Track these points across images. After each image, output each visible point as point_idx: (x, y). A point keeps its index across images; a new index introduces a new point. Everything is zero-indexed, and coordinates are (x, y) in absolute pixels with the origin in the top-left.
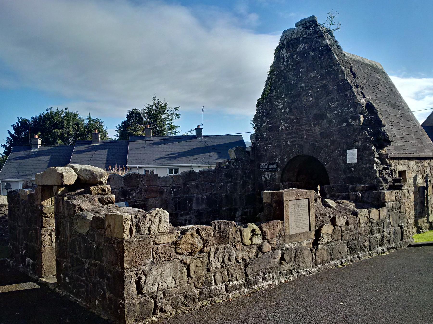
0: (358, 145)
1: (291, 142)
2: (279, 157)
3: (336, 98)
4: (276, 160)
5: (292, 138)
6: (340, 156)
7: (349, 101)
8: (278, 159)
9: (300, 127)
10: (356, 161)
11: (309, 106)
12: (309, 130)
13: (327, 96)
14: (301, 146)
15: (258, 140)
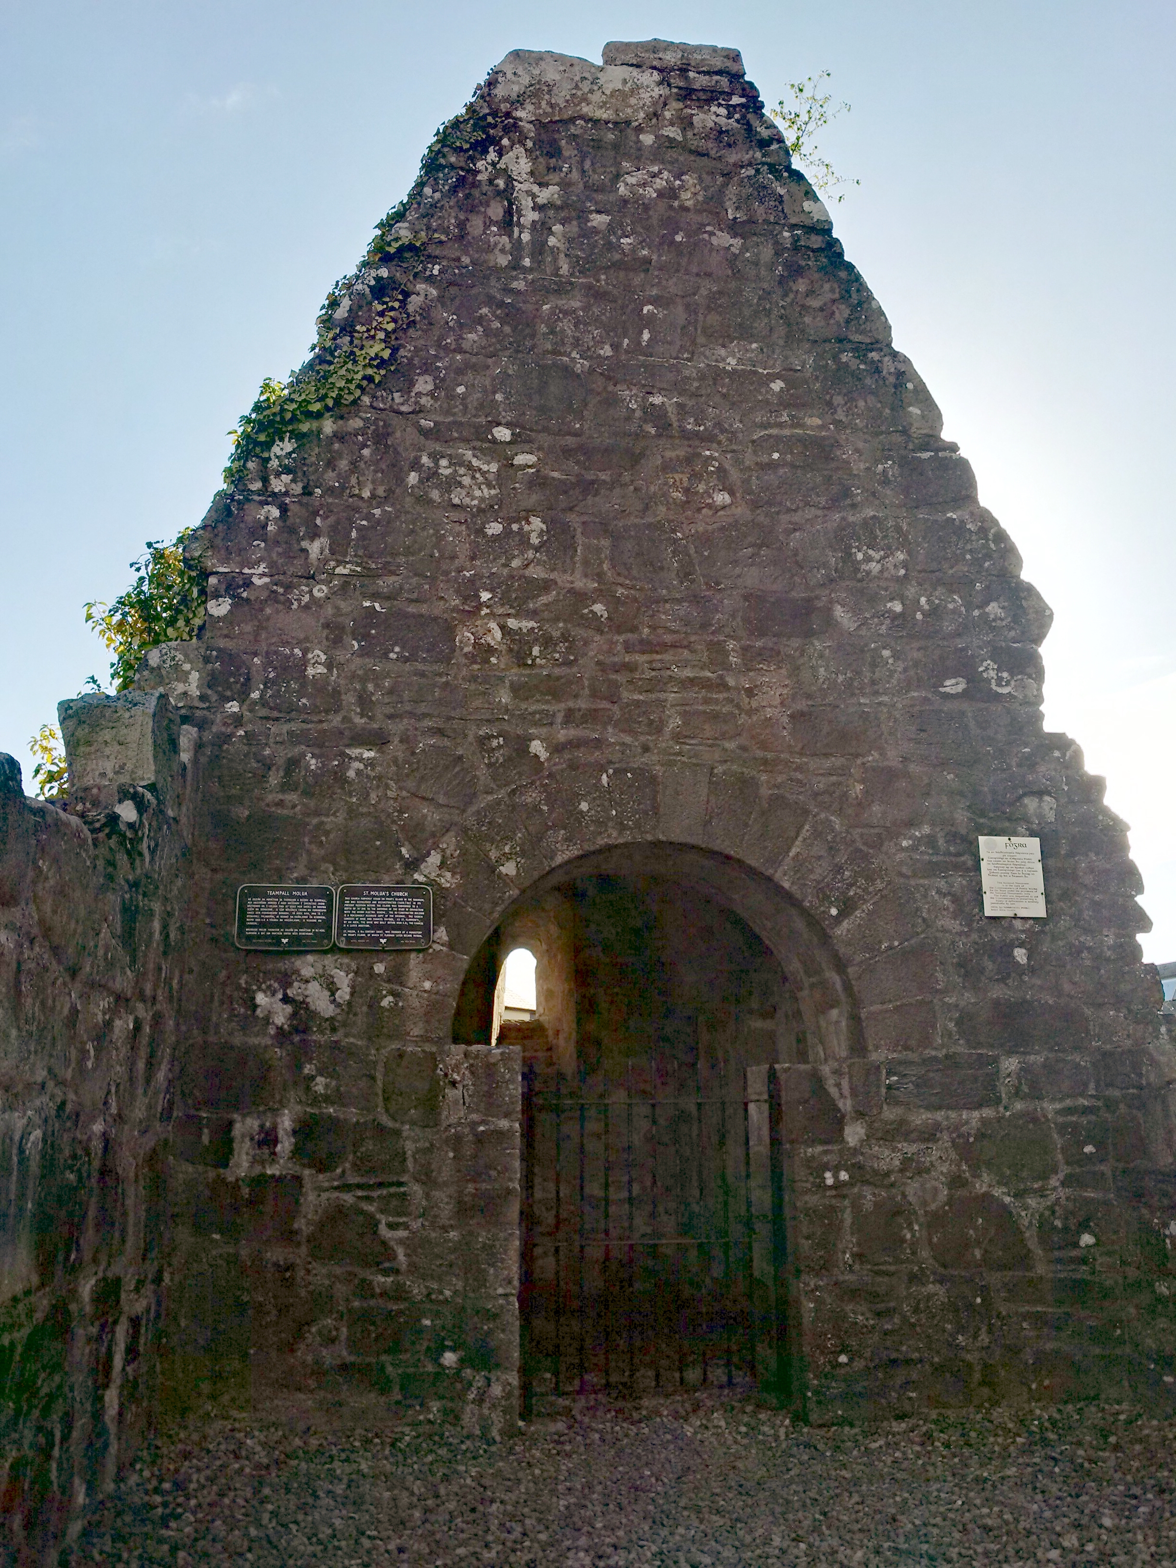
0: (1041, 816)
1: (556, 749)
2: (449, 843)
3: (898, 529)
4: (413, 865)
5: (569, 717)
6: (933, 870)
7: (977, 563)
8: (434, 859)
9: (641, 658)
10: (1040, 911)
11: (705, 540)
12: (706, 684)
13: (834, 503)
14: (647, 780)
15: (242, 696)
